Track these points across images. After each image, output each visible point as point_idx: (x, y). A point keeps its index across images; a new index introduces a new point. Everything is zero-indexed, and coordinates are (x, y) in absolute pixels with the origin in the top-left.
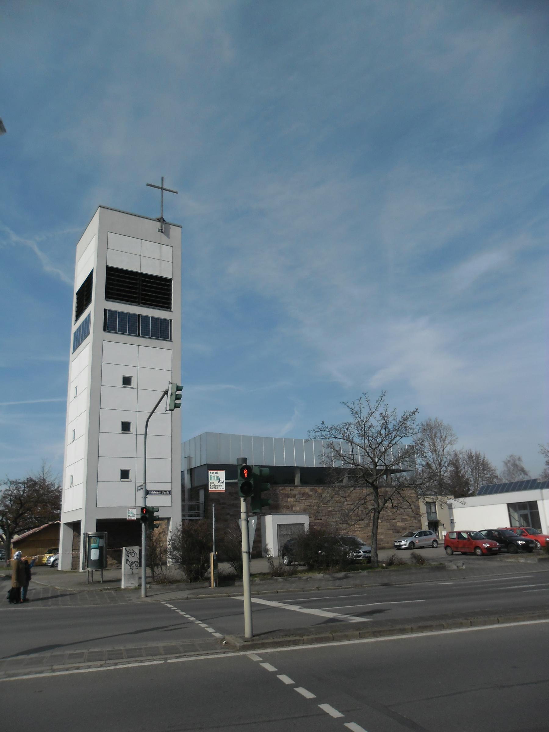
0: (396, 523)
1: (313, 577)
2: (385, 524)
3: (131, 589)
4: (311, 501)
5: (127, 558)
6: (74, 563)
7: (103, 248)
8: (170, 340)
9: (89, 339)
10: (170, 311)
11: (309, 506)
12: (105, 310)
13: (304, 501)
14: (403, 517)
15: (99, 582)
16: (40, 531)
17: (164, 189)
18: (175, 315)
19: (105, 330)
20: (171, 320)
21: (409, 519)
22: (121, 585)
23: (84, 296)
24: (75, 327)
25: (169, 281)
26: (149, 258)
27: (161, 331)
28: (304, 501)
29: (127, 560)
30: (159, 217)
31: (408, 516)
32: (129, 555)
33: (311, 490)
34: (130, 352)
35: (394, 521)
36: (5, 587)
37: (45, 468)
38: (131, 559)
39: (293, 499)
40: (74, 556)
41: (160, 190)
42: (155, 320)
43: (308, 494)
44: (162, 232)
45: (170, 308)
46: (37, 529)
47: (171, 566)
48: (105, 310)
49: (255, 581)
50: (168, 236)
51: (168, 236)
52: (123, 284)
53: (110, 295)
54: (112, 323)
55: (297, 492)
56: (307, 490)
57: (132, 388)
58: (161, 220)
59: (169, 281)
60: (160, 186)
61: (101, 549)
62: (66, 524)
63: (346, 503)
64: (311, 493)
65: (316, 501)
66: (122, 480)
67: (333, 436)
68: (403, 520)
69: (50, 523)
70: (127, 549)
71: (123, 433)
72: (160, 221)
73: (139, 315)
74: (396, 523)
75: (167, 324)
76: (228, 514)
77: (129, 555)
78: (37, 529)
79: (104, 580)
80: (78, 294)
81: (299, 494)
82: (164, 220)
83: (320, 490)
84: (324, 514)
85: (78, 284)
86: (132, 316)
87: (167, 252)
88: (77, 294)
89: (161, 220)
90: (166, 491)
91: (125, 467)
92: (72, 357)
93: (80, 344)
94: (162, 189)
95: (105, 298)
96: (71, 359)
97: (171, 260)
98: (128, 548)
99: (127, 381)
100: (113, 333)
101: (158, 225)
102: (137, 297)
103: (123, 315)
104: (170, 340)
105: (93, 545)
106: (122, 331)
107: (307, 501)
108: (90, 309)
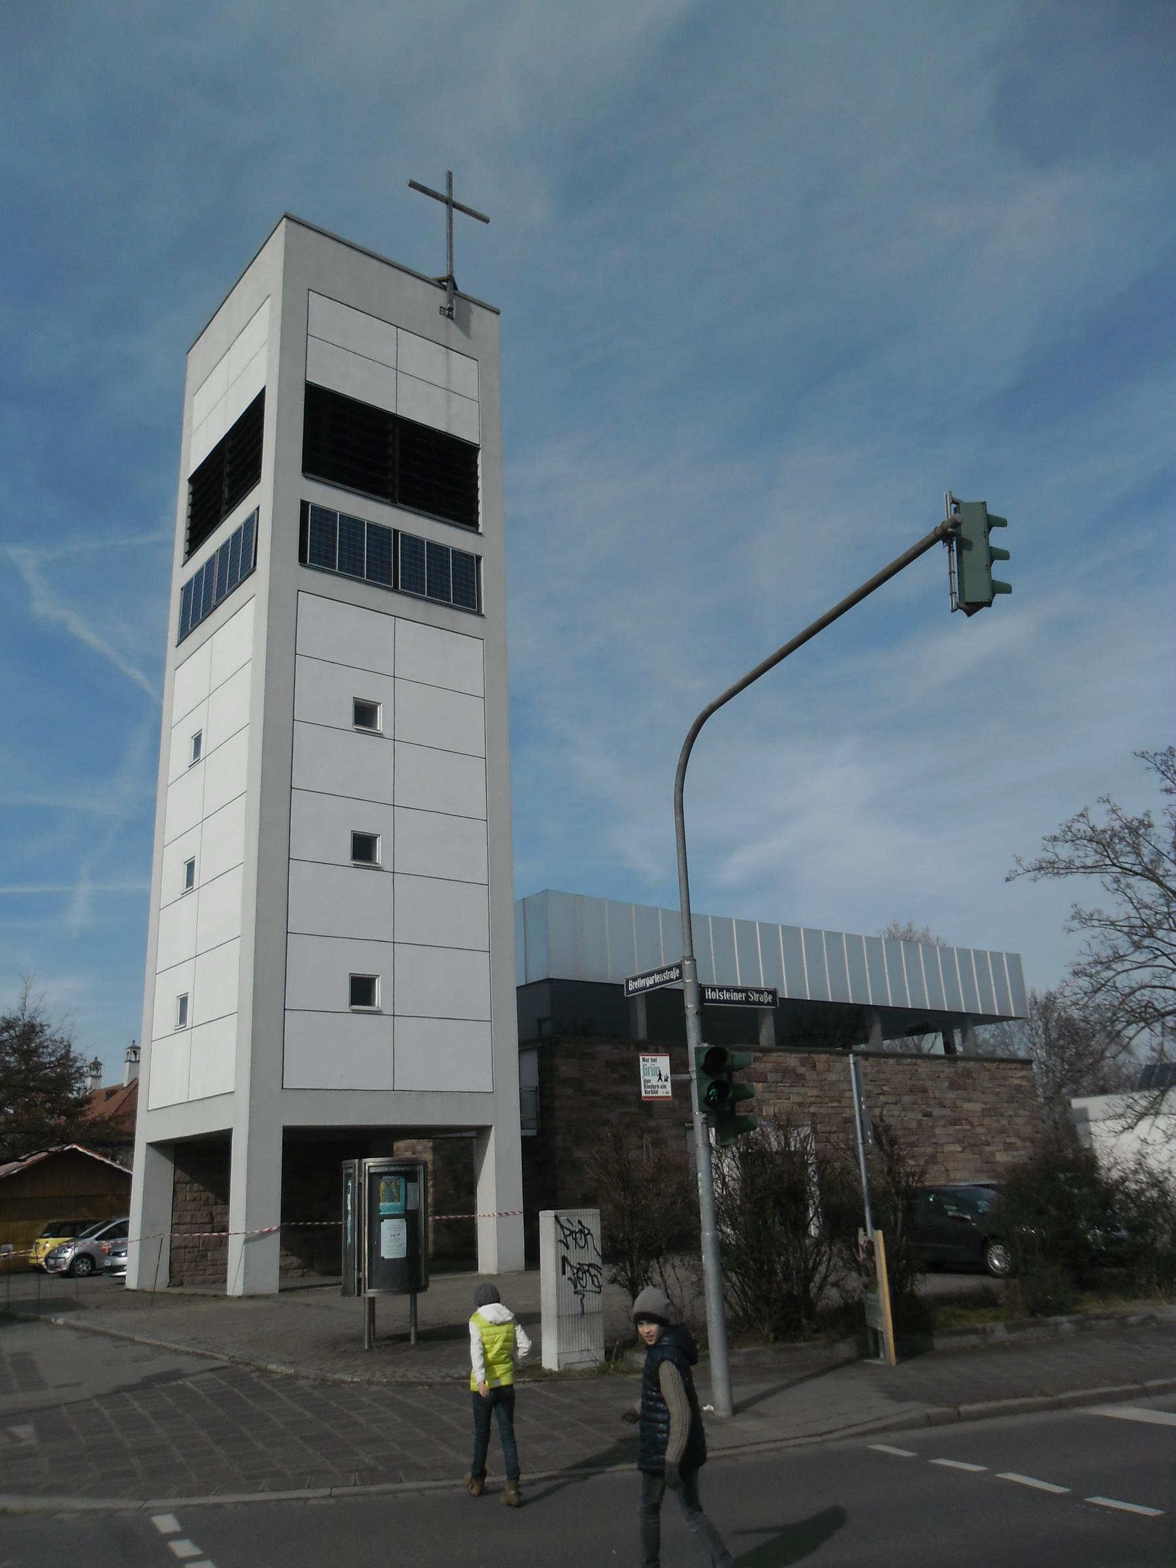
0: (993, 1154)
1: (1158, 1315)
2: (972, 1156)
3: (583, 1373)
4: (802, 1090)
5: (564, 1251)
6: (175, 1265)
7: (295, 334)
8: (479, 613)
9: (256, 586)
10: (476, 532)
11: (799, 1104)
12: (304, 505)
14: (1008, 1140)
15: (405, 1338)
17: (455, 206)
18: (488, 541)
19: (302, 559)
20: (479, 558)
21: (1019, 1143)
23: (231, 469)
24: (183, 573)
25: (470, 451)
26: (419, 383)
27: (451, 584)
29: (565, 1260)
30: (443, 273)
31: (1018, 1136)
32: (570, 1240)
35: (988, 1148)
36: (192, 1382)
37: (29, 1001)
38: (575, 1257)
43: (794, 1070)
44: (450, 317)
45: (477, 526)
48: (304, 505)
49: (993, 1331)
50: (465, 328)
51: (465, 328)
52: (348, 438)
53: (316, 464)
54: (325, 544)
55: (769, 1066)
56: (792, 1060)
57: (380, 735)
58: (447, 283)
59: (470, 451)
61: (411, 1218)
62: (151, 1145)
64: (801, 1070)
66: (355, 1007)
67: (1108, 861)
68: (1009, 1147)
69: (53, 1149)
70: (563, 1219)
71: (356, 866)
72: (444, 288)
73: (396, 532)
75: (468, 565)
76: (606, 1122)
77: (570, 1240)
79: (421, 1328)
81: (776, 1071)
84: (834, 1129)
85: (200, 441)
86: (375, 529)
87: (465, 372)
88: (192, 480)
89: (447, 283)
90: (760, 992)
91: (363, 970)
92: (173, 654)
93: (209, 610)
94: (451, 204)
95: (303, 471)
96: (170, 663)
98: (564, 1215)
99: (364, 714)
100: (323, 571)
101: (440, 297)
102: (390, 483)
103: (352, 525)
104: (479, 613)
105: (385, 1206)
106: (350, 569)
107: (795, 1090)
108: (260, 498)
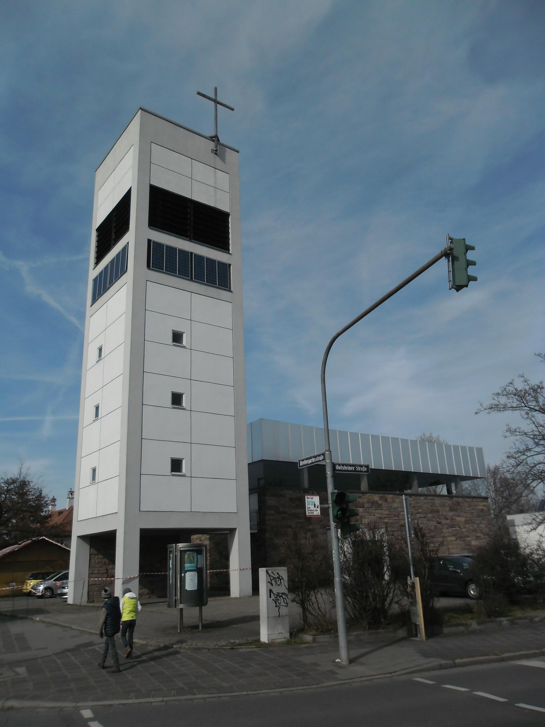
0: (470, 541)
2: (460, 542)
3: (279, 644)
4: (381, 511)
5: (270, 587)
7: (145, 162)
8: (230, 291)
10: (228, 253)
13: (374, 511)
14: (478, 535)
15: (197, 627)
16: (20, 550)
17: (219, 103)
19: (148, 266)
20: (230, 265)
21: (482, 536)
22: (258, 633)
23: (116, 224)
24: (94, 273)
26: (202, 184)
27: (217, 277)
28: (374, 511)
29: (271, 591)
30: (213, 134)
31: (482, 533)
32: (273, 582)
33: (381, 499)
34: (179, 300)
35: (468, 539)
37: (23, 470)
38: (276, 590)
39: (361, 509)
40: (90, 583)
41: (213, 103)
42: (211, 262)
43: (377, 502)
44: (216, 154)
45: (229, 250)
46: (15, 547)
47: (335, 602)
49: (471, 625)
50: (223, 159)
51: (223, 159)
52: (170, 210)
53: (156, 221)
54: (159, 259)
55: (365, 500)
56: (376, 497)
57: (184, 347)
58: (215, 139)
60: (213, 96)
61: (199, 571)
62: (83, 538)
63: (418, 515)
64: (380, 502)
65: (387, 512)
67: (523, 405)
68: (478, 538)
69: (34, 539)
70: (270, 572)
71: (173, 408)
72: (213, 141)
73: (192, 253)
74: (470, 541)
75: (225, 268)
76: (290, 527)
77: (273, 582)
78: (15, 547)
79: (204, 622)
80: (99, 230)
81: (368, 502)
82: (219, 140)
83: (390, 497)
86: (183, 253)
93: (106, 290)
94: (216, 102)
96: (88, 314)
97: (227, 189)
98: (270, 570)
102: (189, 231)
103: (171, 250)
104: (230, 291)
105: (187, 566)
106: (171, 270)
107: (377, 511)
